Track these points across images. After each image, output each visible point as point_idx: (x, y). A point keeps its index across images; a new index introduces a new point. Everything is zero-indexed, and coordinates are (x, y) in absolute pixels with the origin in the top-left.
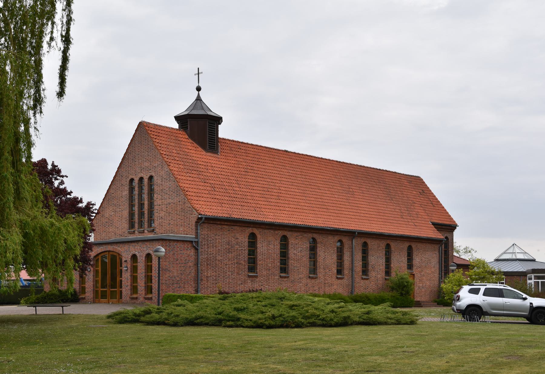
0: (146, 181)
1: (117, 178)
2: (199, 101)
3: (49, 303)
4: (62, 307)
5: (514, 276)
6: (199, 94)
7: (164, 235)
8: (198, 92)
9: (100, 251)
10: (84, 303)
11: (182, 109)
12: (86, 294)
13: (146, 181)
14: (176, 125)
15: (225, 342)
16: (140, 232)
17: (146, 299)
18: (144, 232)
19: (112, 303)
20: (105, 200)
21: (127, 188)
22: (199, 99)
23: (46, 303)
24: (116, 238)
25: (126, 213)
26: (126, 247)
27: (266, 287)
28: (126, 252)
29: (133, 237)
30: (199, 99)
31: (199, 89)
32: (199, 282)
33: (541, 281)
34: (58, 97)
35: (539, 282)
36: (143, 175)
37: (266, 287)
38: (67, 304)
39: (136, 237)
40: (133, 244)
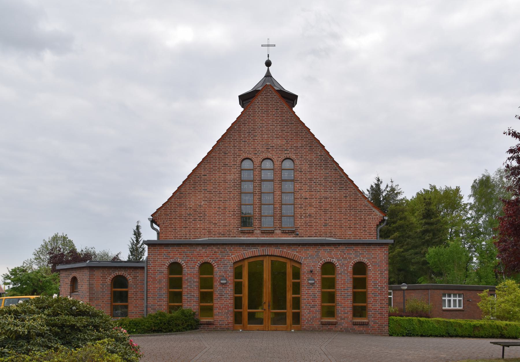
2: (267, 78)
3: (176, 332)
5: (428, 289)
6: (268, 70)
8: (267, 67)
10: (210, 331)
12: (216, 317)
15: (514, 349)
19: (510, 312)
22: (268, 75)
23: (171, 331)
26: (311, 251)
29: (270, 238)
30: (268, 75)
31: (268, 64)
38: (364, 319)
39: (256, 238)
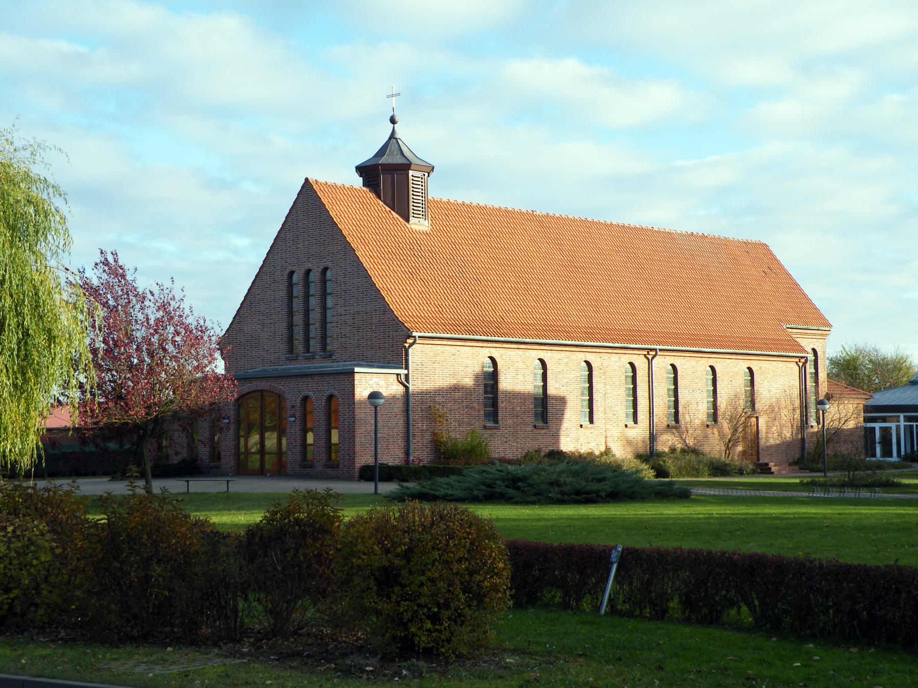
0: (314, 277)
1: (265, 269)
4: (188, 481)
6: (393, 132)
7: (350, 363)
9: (247, 391)
11: (366, 154)
13: (314, 277)
14: (357, 181)
16: (306, 358)
17: (328, 468)
18: (314, 358)
20: (244, 305)
21: (283, 286)
22: (393, 136)
24: (263, 368)
25: (282, 326)
27: (513, 444)
28: (292, 393)
32: (411, 438)
33: (881, 428)
34: (480, 444)
35: (874, 428)
36: (311, 265)
37: (513, 444)
40: (305, 379)
